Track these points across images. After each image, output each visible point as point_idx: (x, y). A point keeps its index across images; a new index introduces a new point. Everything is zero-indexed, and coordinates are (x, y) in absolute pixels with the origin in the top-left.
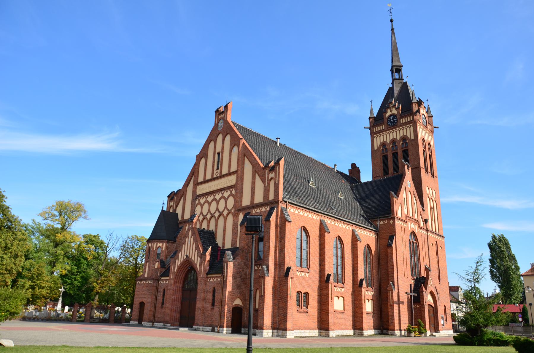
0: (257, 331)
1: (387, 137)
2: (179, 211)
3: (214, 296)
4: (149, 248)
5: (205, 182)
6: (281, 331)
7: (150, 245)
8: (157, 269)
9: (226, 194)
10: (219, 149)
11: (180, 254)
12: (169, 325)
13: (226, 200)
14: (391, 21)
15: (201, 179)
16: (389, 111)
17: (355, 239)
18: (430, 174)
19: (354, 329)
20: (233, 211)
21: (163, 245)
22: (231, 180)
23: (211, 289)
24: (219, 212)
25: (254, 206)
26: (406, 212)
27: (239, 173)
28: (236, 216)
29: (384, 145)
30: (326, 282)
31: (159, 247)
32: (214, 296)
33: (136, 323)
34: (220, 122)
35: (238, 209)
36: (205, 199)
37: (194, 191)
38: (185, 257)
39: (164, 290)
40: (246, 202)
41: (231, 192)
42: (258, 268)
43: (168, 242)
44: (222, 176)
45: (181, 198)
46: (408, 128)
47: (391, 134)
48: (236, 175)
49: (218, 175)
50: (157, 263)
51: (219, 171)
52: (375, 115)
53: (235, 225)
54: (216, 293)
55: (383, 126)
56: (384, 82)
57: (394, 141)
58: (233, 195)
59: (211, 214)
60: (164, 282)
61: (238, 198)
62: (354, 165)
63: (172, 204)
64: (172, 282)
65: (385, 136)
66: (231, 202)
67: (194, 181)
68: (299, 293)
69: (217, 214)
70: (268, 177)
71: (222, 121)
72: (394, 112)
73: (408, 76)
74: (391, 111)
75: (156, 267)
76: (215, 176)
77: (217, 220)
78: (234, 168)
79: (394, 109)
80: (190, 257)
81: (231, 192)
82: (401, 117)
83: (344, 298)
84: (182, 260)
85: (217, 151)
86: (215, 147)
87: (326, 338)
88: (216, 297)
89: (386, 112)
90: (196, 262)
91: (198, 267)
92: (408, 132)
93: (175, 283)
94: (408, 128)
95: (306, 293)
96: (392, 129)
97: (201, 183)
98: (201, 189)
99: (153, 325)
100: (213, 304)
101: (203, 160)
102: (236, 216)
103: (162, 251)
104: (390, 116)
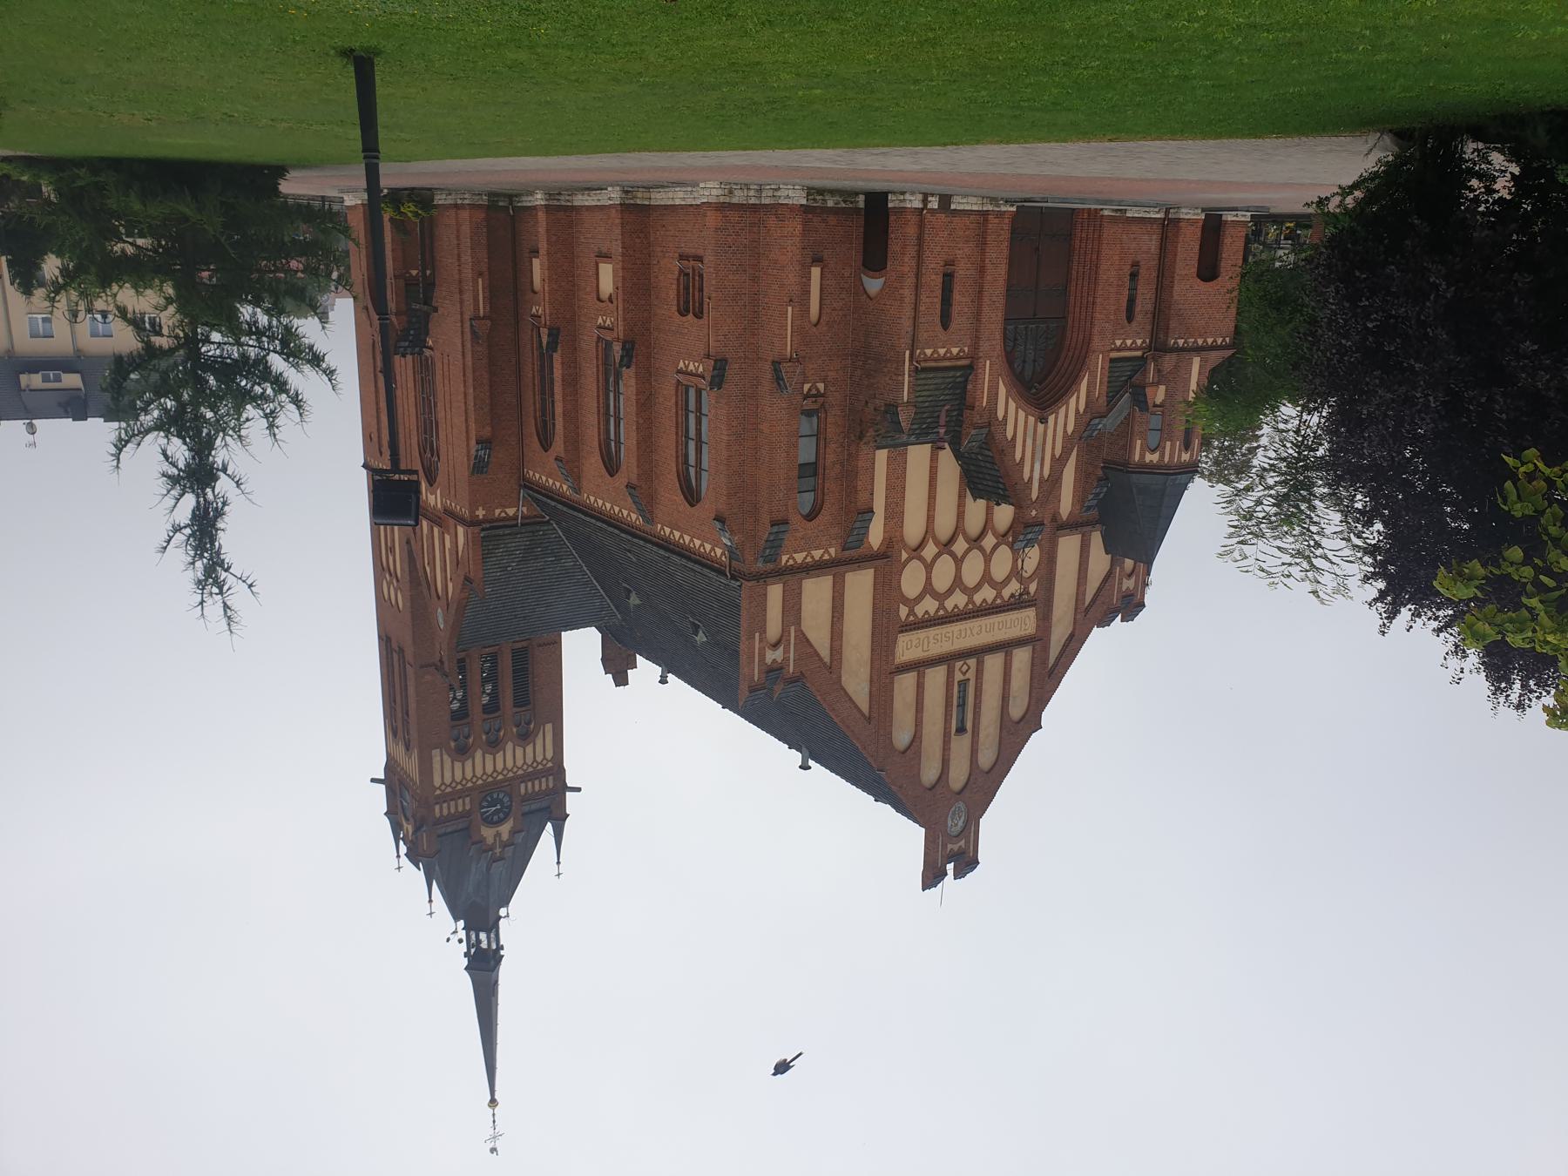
0: (804, 202)
1: (512, 758)
2: (1099, 561)
3: (946, 301)
4: (1187, 446)
5: (1006, 647)
6: (735, 200)
7: (1185, 457)
8: (1159, 383)
9: (929, 606)
10: (961, 745)
11: (1070, 429)
12: (1106, 213)
13: (928, 589)
14: (493, 1102)
15: (1022, 657)
16: (505, 837)
17: (571, 467)
18: (395, 646)
19: (885, 212)
20: (904, 556)
21: (1142, 456)
22: (909, 647)
23: (960, 320)
24: (953, 555)
25: (835, 567)
26: (447, 537)
27: (885, 669)
28: (893, 541)
29: (525, 737)
30: (633, 343)
31: (1153, 451)
32: (946, 301)
33: (1229, 217)
34: (959, 828)
35: (886, 561)
36: (1006, 593)
37: (1045, 618)
38: (1051, 419)
39: (1130, 319)
40: (860, 584)
41: (911, 612)
42: (814, 386)
43: (1126, 464)
44: (948, 659)
45: (1094, 600)
46: (448, 781)
47: (500, 767)
48: (897, 661)
49: (959, 664)
50: (1158, 402)
51: (958, 677)
52: (549, 826)
53: (895, 513)
54: (938, 306)
55: (523, 791)
56: (518, 924)
57: (494, 745)
58: (906, 601)
59: (982, 550)
60: (1133, 342)
61: (887, 591)
62: (621, 680)
63: (1129, 584)
64: (1096, 342)
65: (520, 763)
66: (911, 580)
67: (1046, 649)
68: (699, 315)
69: (960, 546)
70: (786, 651)
71: (955, 830)
72: (488, 833)
73: (438, 934)
74: (498, 834)
75: (1162, 388)
76: (972, 662)
77: (959, 529)
78: (906, 683)
79: (490, 840)
80: (1032, 419)
81: (911, 612)
82: (466, 815)
83: (599, 299)
84: (1062, 411)
85: (966, 739)
86: (974, 751)
87: (817, 183)
88: (938, 301)
89: (513, 832)
90: (1012, 405)
91: (1002, 390)
92: (447, 771)
93: (1087, 341)
94: (448, 781)
95: (683, 312)
96: (495, 782)
97: (1020, 642)
98: (1022, 623)
99: (1167, 212)
100: (948, 278)
101: (1016, 711)
102: (893, 541)
103: (1144, 439)
104: (500, 822)
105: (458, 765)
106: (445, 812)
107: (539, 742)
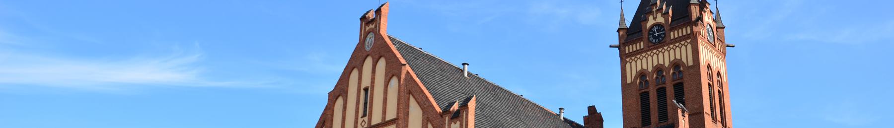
1: (648, 62)
10: (366, 82)
16: (651, 18)
29: (642, 75)
34: (369, 36)
46: (683, 48)
47: (655, 57)
51: (366, 119)
52: (628, 25)
55: (642, 43)
57: (659, 69)
65: (644, 60)
71: (371, 35)
74: (655, 19)
78: (391, 114)
79: (659, 15)
82: (672, 29)
85: (363, 86)
92: (683, 53)
94: (683, 48)
96: (657, 48)
101: (340, 101)
104: (652, 27)
105: (678, 57)
106: (684, 30)
107: (634, 73)
